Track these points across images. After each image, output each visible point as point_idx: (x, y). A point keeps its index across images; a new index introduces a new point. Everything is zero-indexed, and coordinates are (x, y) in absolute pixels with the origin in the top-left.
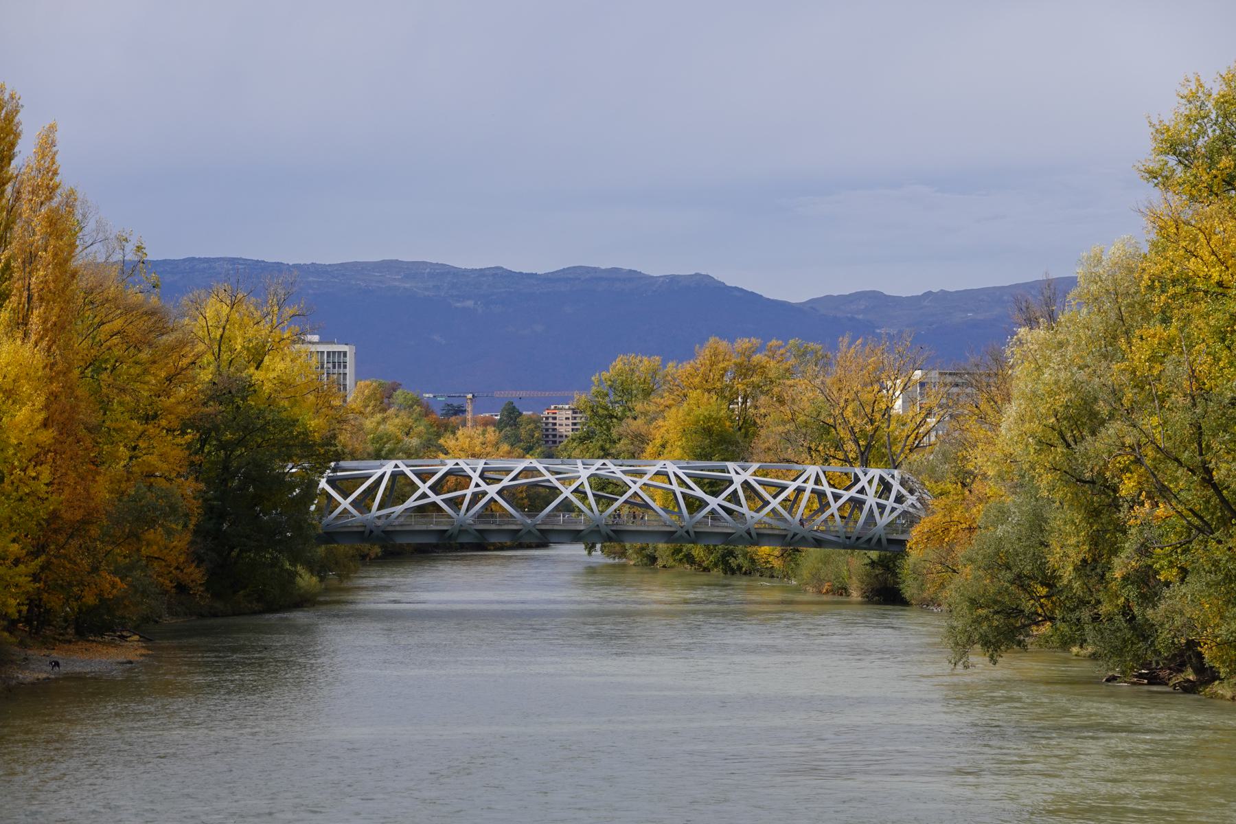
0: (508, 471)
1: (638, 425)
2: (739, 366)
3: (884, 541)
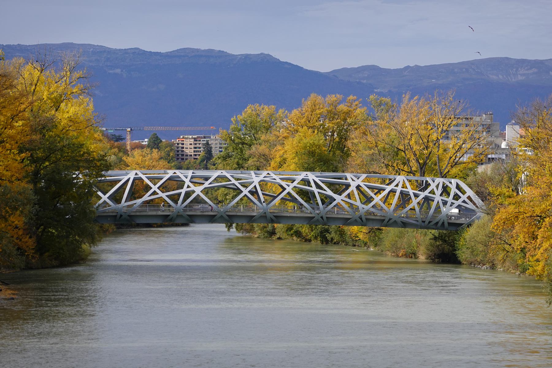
0: (207, 179)
1: (263, 149)
2: (329, 112)
3: (446, 224)
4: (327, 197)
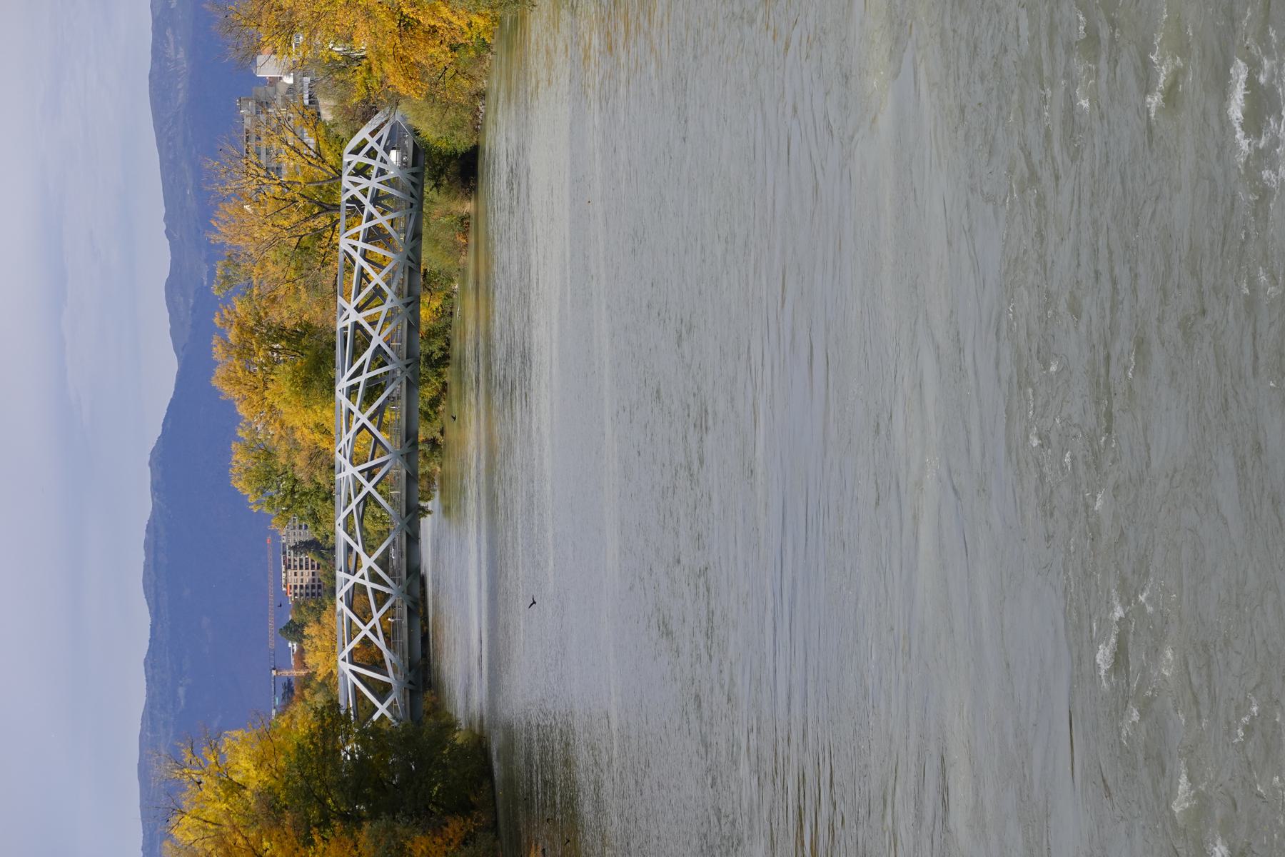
0: (349, 549)
1: (300, 461)
3: (415, 170)
4: (375, 357)
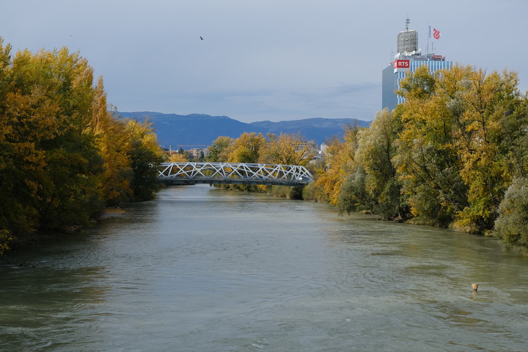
1: (224, 154)
